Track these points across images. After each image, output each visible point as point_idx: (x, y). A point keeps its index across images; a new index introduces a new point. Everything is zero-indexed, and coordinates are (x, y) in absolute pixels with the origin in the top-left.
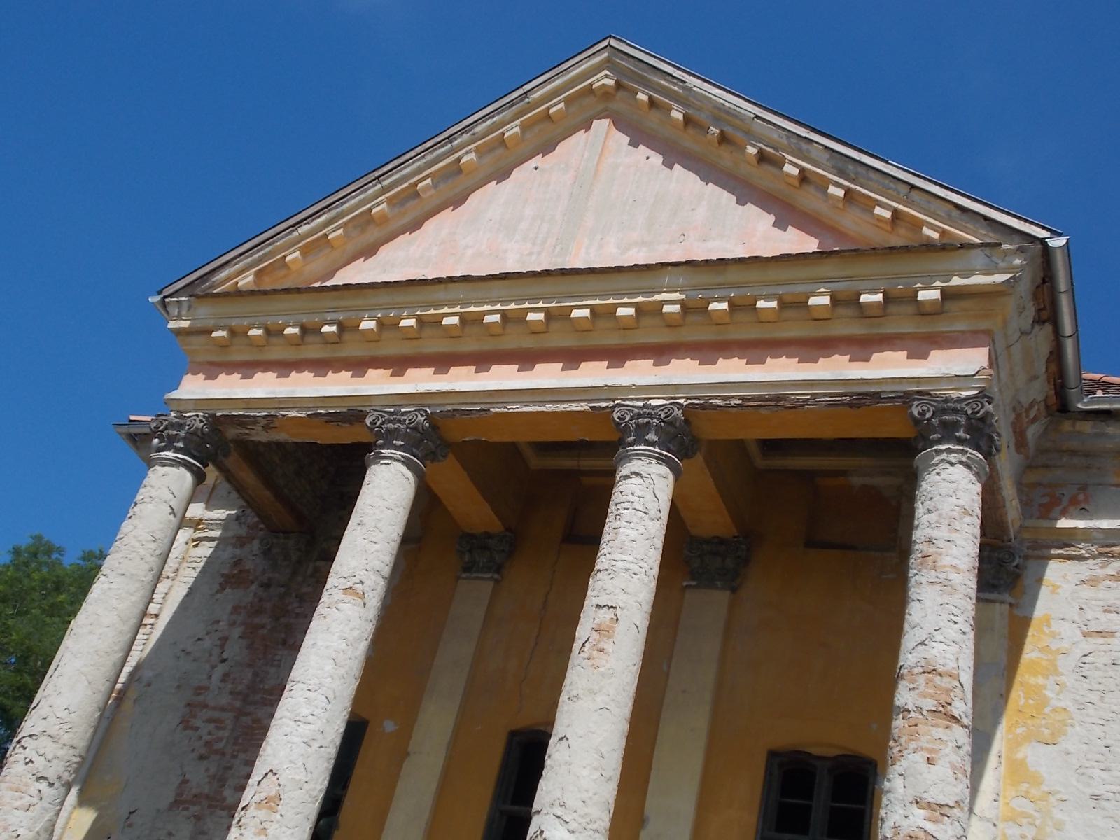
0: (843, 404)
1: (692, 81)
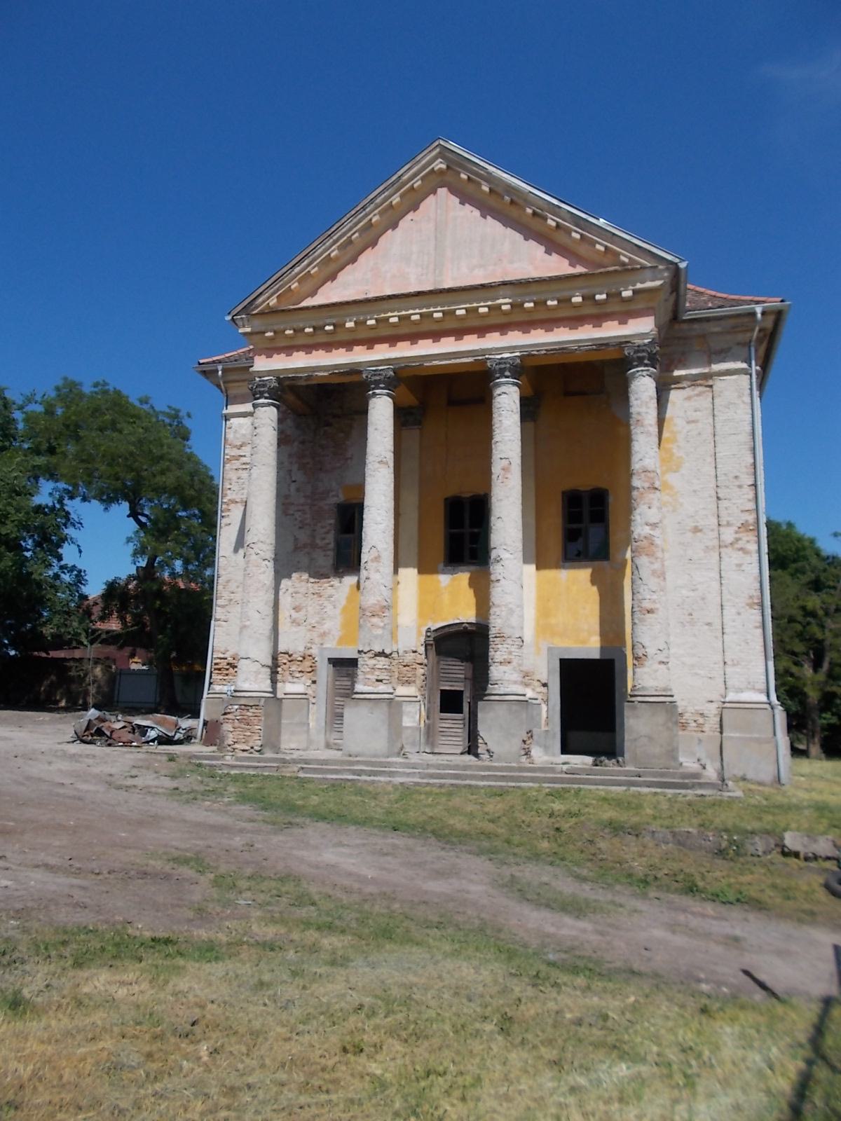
0: (593, 350)
1: (491, 169)
